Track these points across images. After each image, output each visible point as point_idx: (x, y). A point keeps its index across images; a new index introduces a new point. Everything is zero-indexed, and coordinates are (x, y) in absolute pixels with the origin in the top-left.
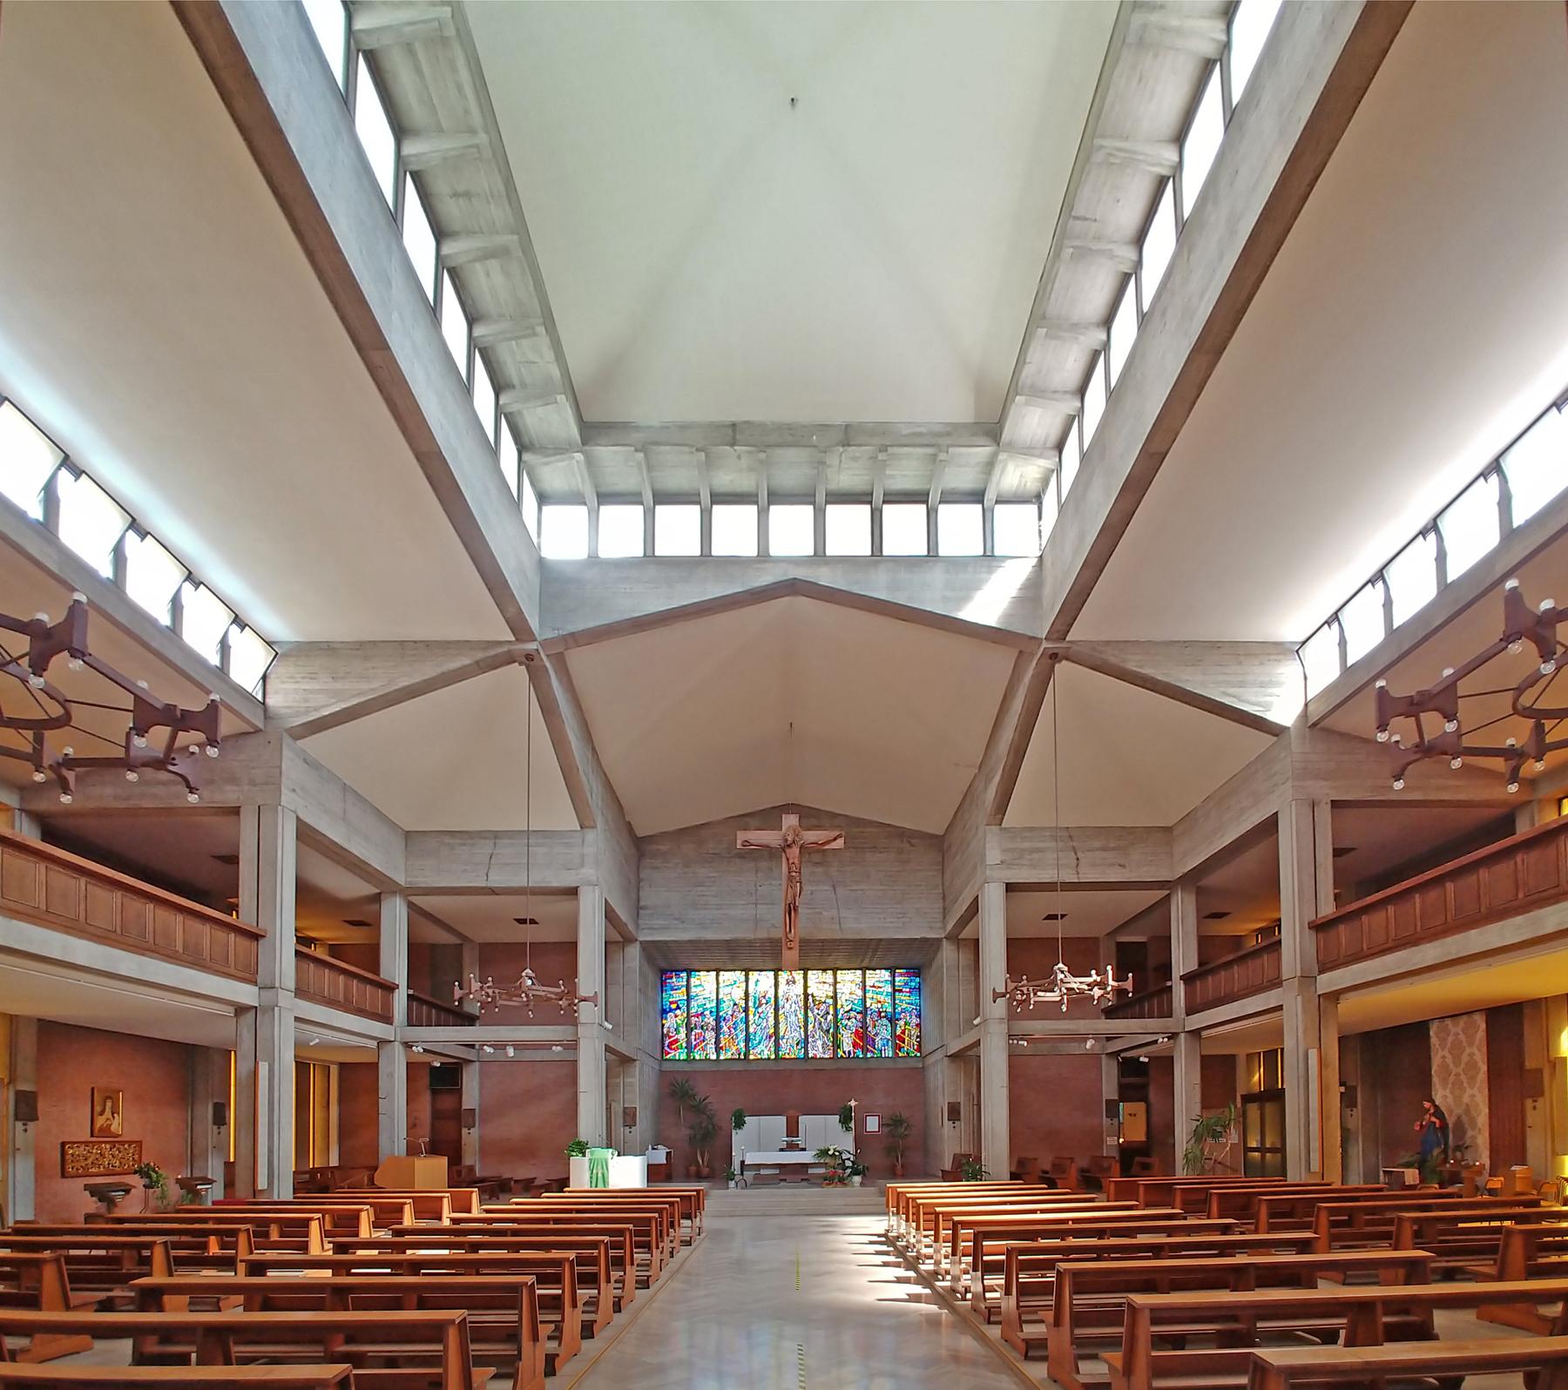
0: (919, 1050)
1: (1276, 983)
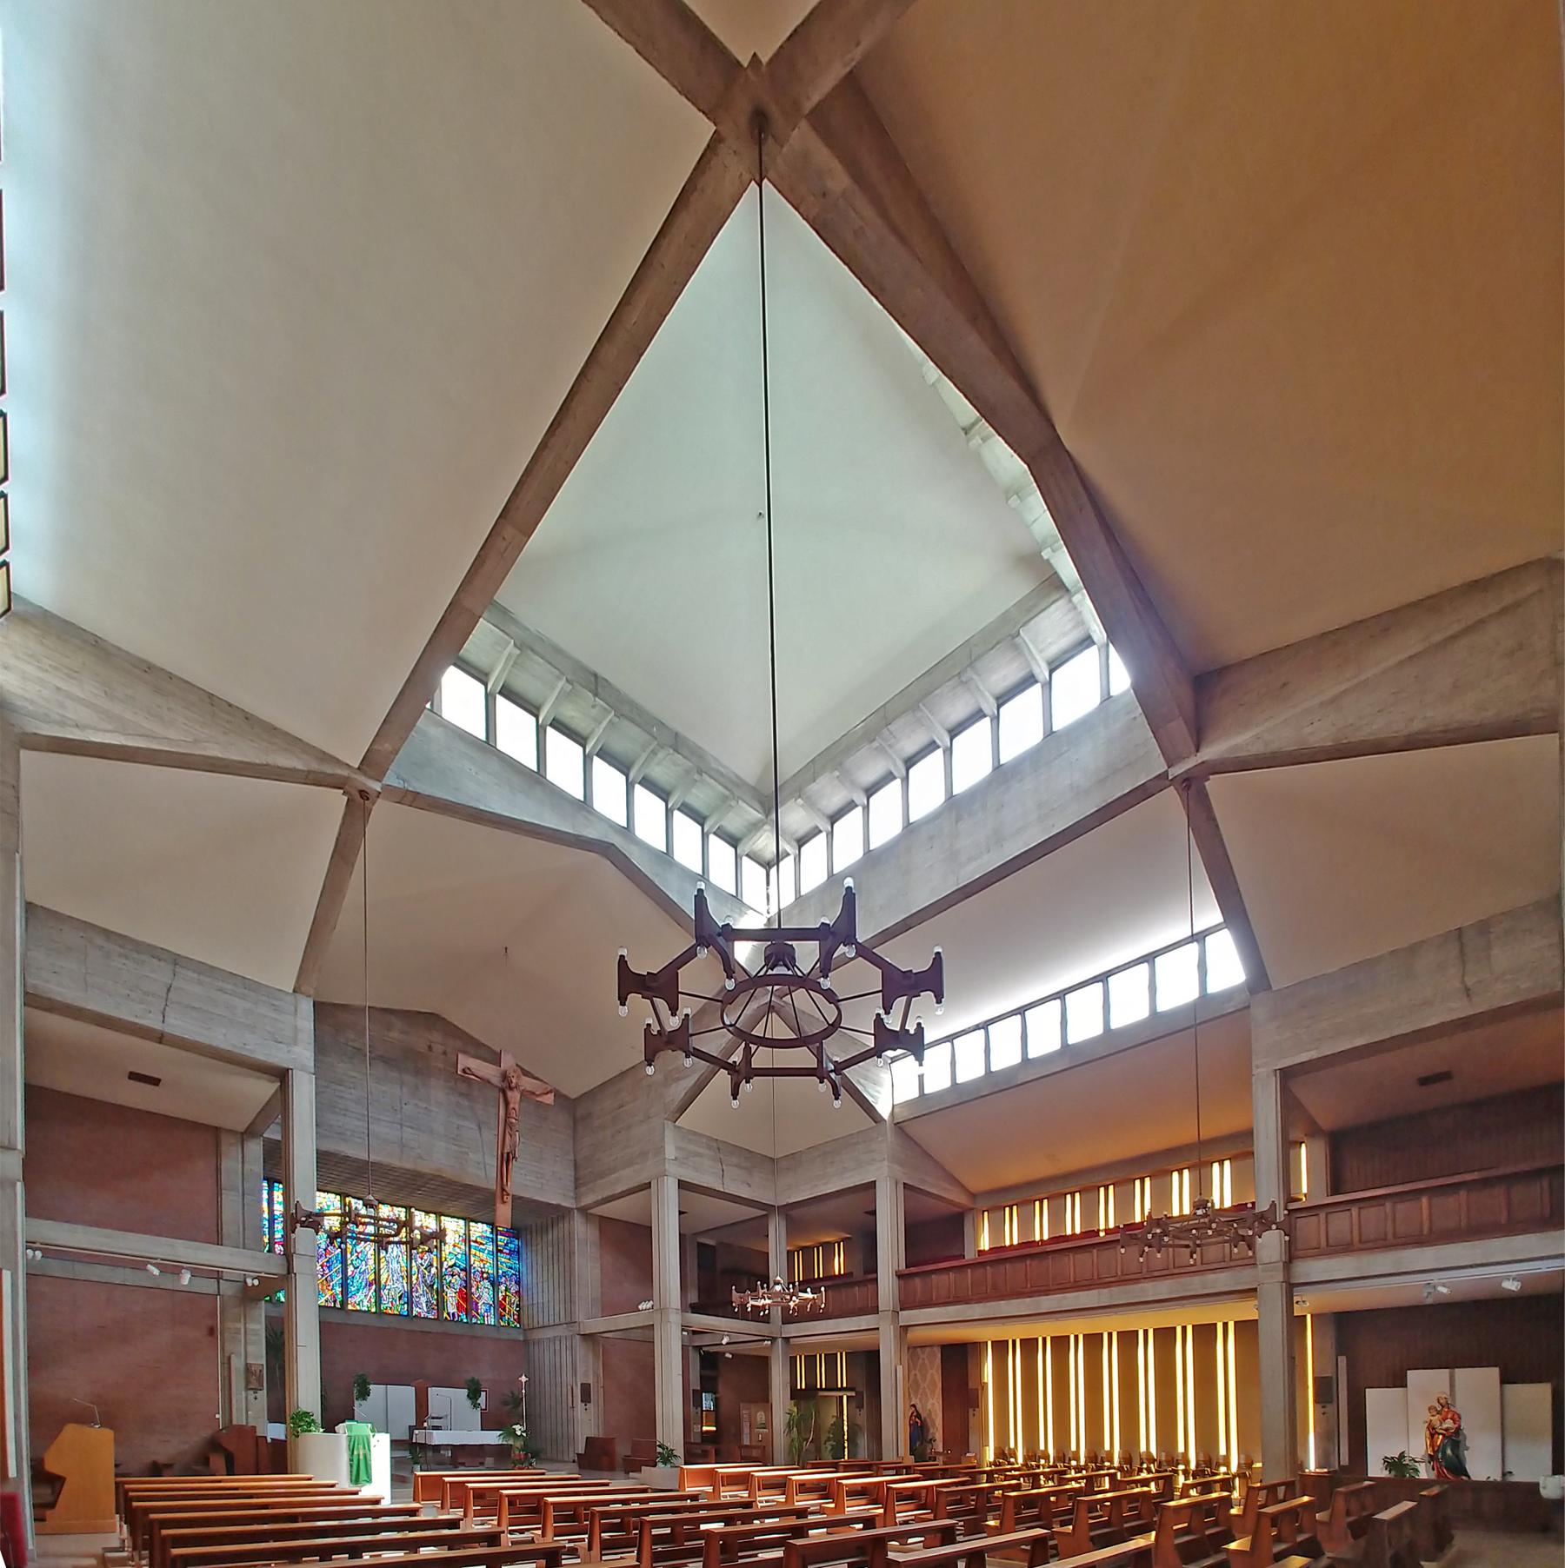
1: (875, 1310)
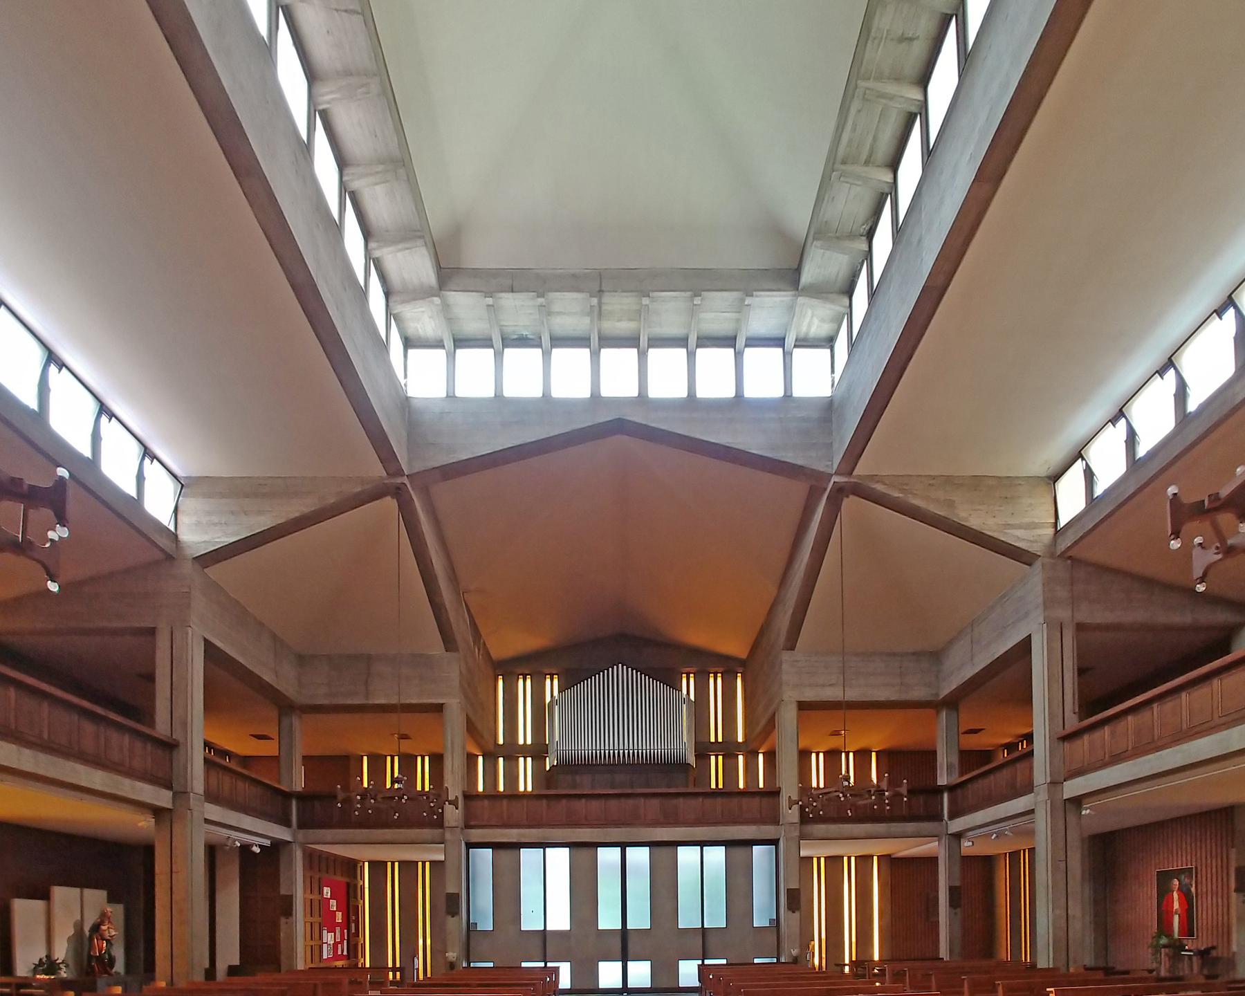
1: (1028, 788)
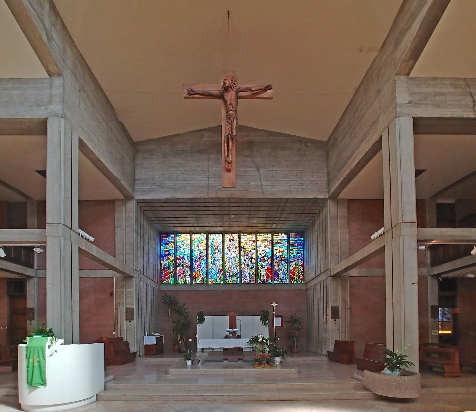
0: (303, 279)
